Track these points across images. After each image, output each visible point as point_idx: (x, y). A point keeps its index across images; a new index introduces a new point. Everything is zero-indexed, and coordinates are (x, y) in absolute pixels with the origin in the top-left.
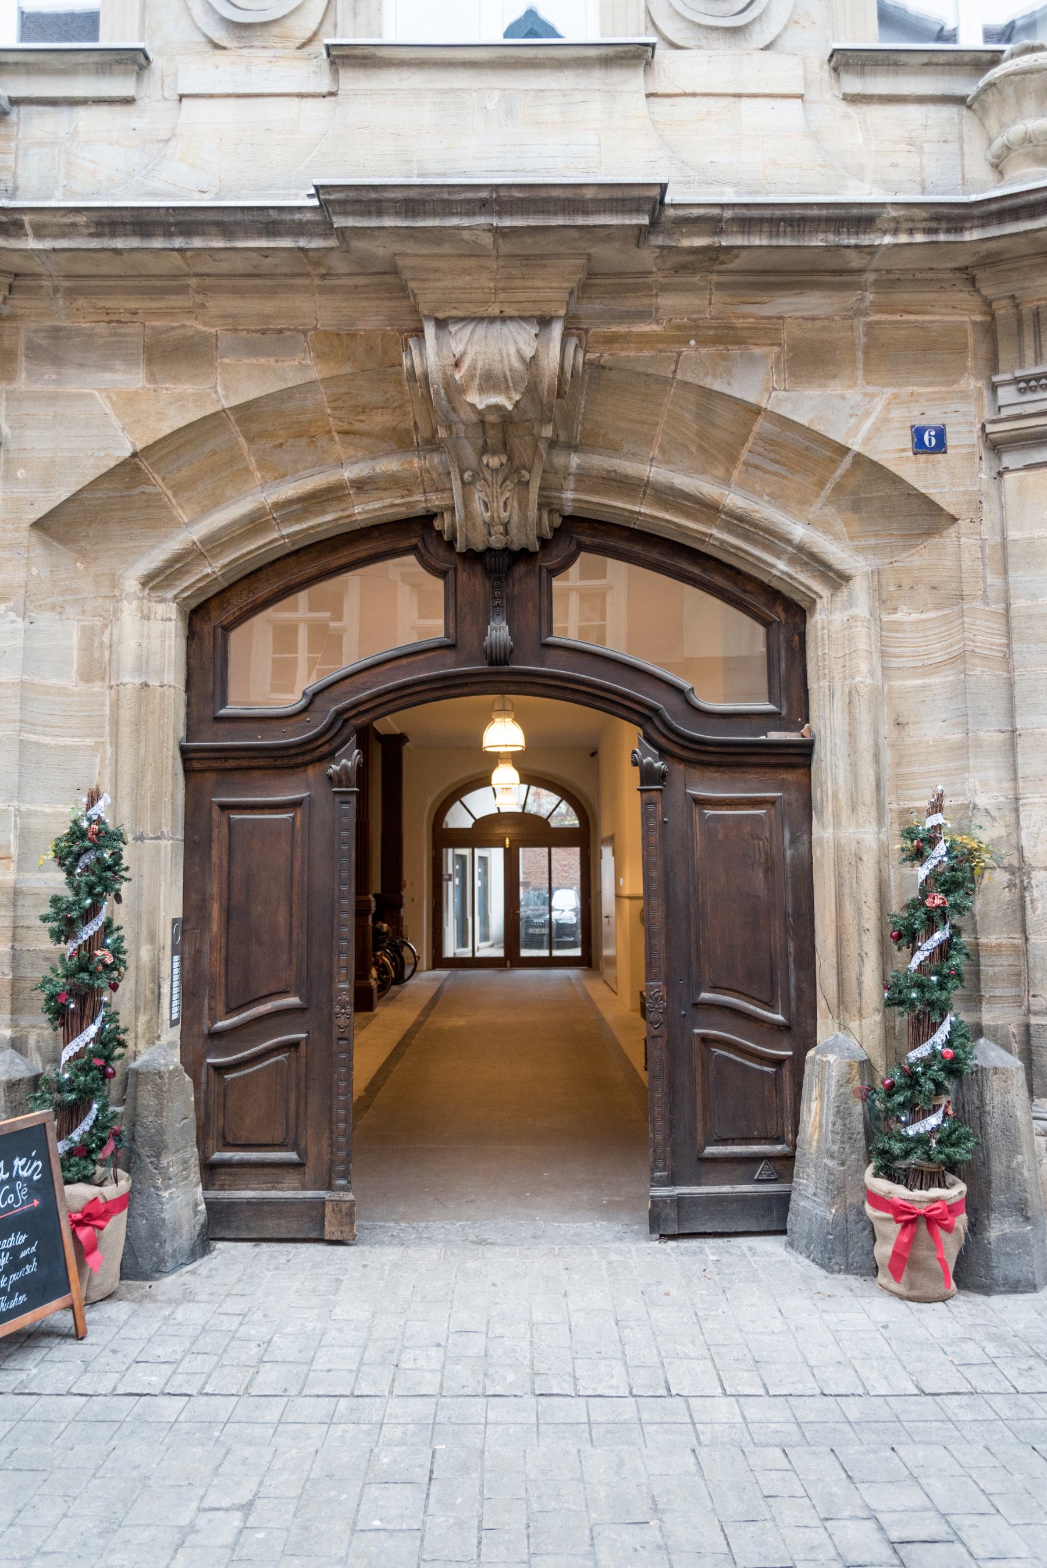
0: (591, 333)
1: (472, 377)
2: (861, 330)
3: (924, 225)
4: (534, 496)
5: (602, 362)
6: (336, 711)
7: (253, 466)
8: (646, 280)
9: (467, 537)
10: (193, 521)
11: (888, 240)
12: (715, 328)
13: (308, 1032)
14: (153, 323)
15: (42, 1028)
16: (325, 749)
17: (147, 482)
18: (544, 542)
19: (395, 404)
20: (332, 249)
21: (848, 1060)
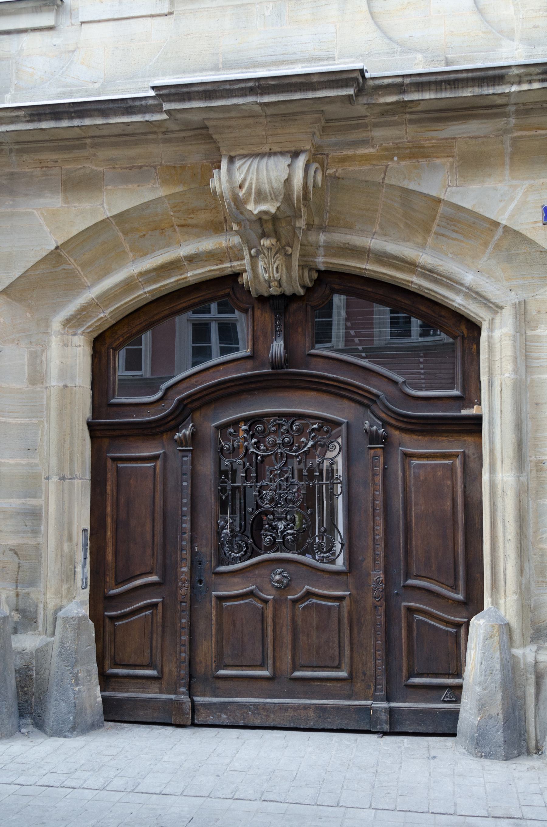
0: (330, 156)
1: (249, 193)
2: (509, 142)
3: (540, 77)
4: (295, 261)
5: (337, 175)
6: (178, 400)
7: (128, 249)
8: (363, 121)
9: (255, 289)
10: (93, 285)
11: (514, 88)
12: (411, 148)
13: (163, 598)
14: (67, 167)
15: (10, 590)
16: (173, 423)
17: (66, 263)
18: (308, 290)
19: (212, 207)
20: (166, 120)
21: (492, 624)
